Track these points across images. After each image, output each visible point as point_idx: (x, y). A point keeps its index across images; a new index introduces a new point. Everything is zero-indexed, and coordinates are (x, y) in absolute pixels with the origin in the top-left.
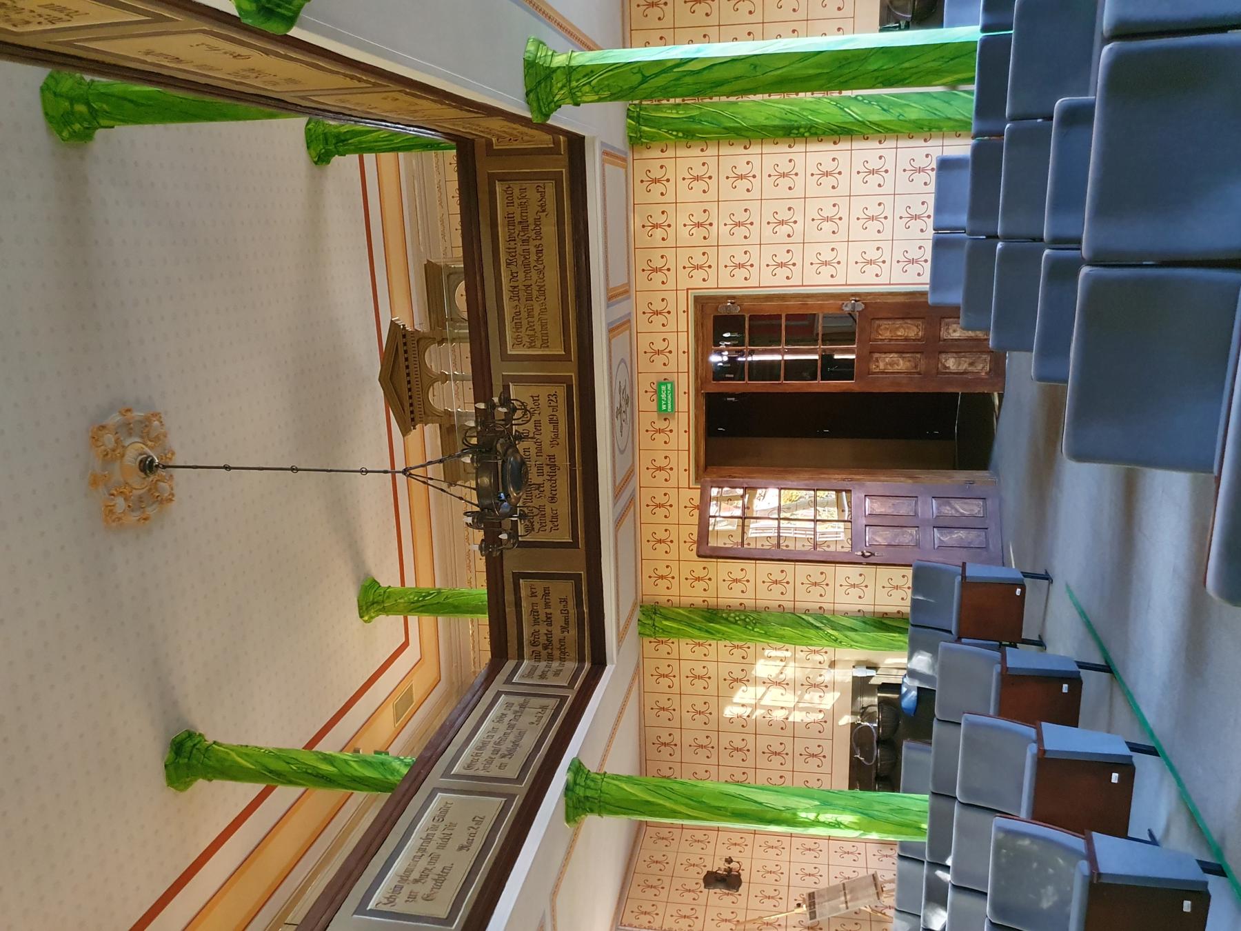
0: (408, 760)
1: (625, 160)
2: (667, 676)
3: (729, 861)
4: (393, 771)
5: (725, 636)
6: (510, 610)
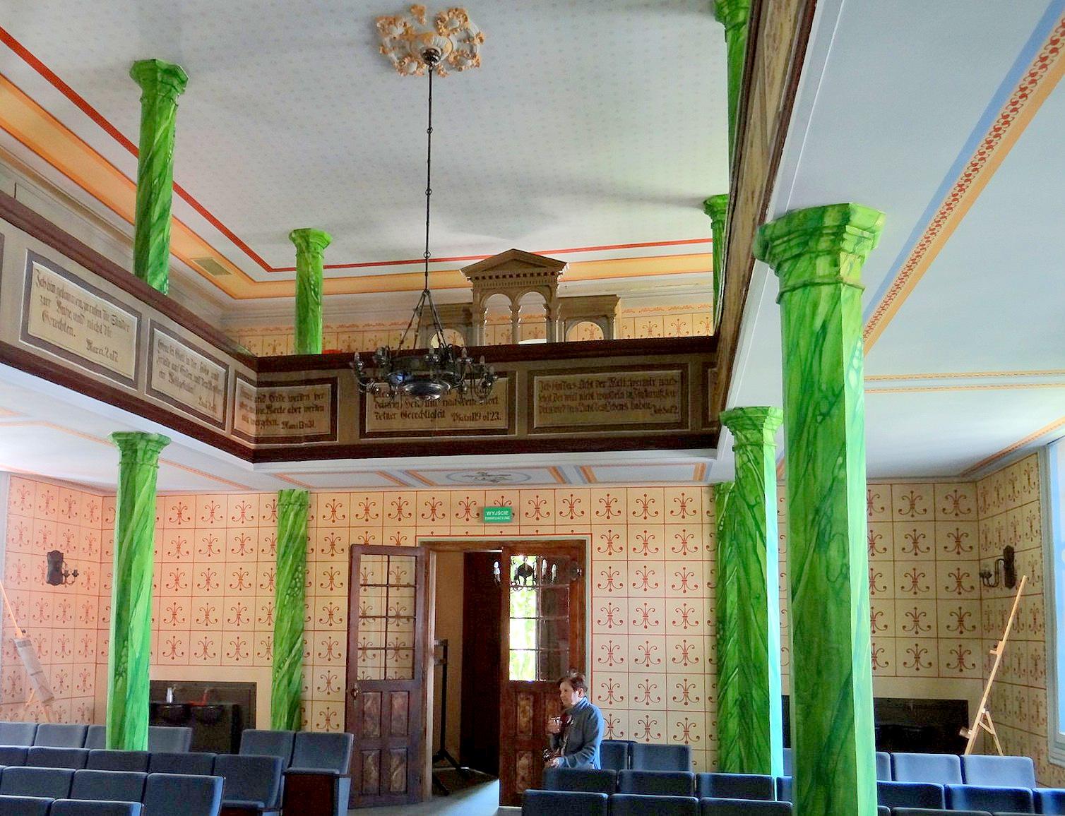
0: (166, 288)
1: (700, 480)
3: (75, 574)
4: (155, 274)
5: (280, 570)
6: (303, 375)
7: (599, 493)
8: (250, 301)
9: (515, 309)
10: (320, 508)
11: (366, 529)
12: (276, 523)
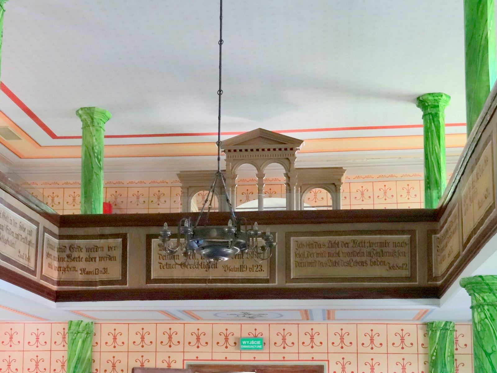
2: (37, 341)
6: (98, 230)
7: (334, 327)
8: (34, 160)
9: (261, 176)
10: (104, 336)
11: (141, 354)
12: (66, 347)
